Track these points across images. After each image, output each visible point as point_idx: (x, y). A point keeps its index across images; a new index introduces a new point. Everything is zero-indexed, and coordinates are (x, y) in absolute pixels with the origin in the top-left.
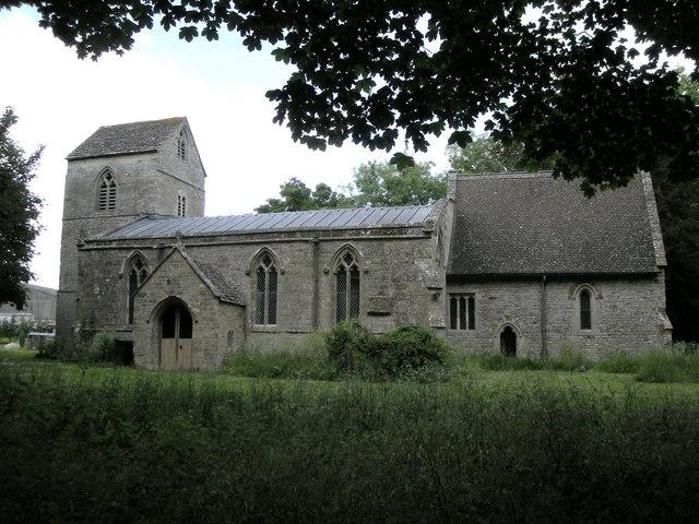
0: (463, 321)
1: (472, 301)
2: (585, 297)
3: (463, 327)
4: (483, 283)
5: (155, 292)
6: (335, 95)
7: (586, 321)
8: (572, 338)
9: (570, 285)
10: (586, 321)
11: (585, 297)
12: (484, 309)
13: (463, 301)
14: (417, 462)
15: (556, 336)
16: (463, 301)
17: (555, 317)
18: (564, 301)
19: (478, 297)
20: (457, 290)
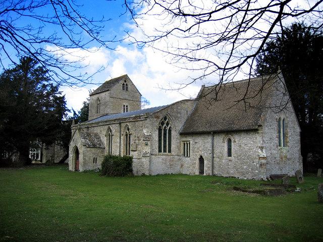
0: (165, 147)
1: (190, 143)
2: (230, 141)
3: (165, 151)
4: (302, 154)
5: (298, 178)
6: (261, 69)
7: (230, 154)
8: (224, 161)
9: (224, 136)
10: (230, 154)
11: (230, 141)
12: (193, 147)
13: (187, 144)
14: (46, 149)
15: (218, 160)
16: (187, 144)
17: (217, 151)
18: (221, 144)
19: (191, 142)
20: (184, 139)
